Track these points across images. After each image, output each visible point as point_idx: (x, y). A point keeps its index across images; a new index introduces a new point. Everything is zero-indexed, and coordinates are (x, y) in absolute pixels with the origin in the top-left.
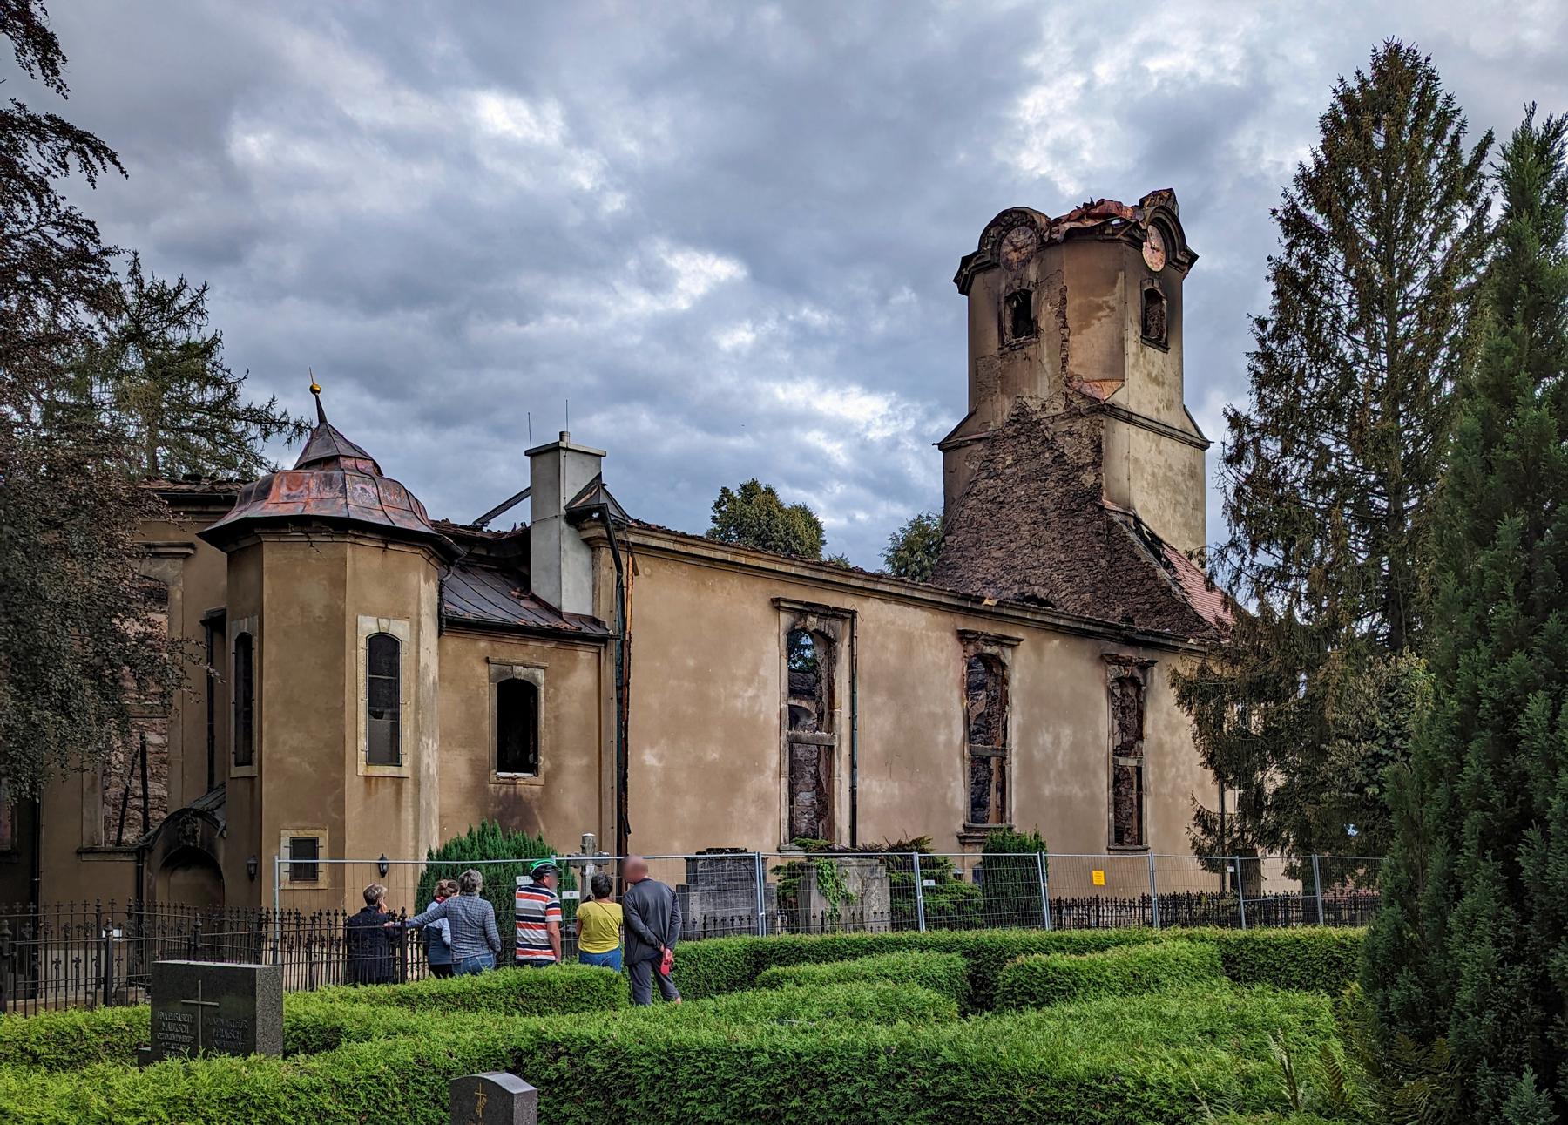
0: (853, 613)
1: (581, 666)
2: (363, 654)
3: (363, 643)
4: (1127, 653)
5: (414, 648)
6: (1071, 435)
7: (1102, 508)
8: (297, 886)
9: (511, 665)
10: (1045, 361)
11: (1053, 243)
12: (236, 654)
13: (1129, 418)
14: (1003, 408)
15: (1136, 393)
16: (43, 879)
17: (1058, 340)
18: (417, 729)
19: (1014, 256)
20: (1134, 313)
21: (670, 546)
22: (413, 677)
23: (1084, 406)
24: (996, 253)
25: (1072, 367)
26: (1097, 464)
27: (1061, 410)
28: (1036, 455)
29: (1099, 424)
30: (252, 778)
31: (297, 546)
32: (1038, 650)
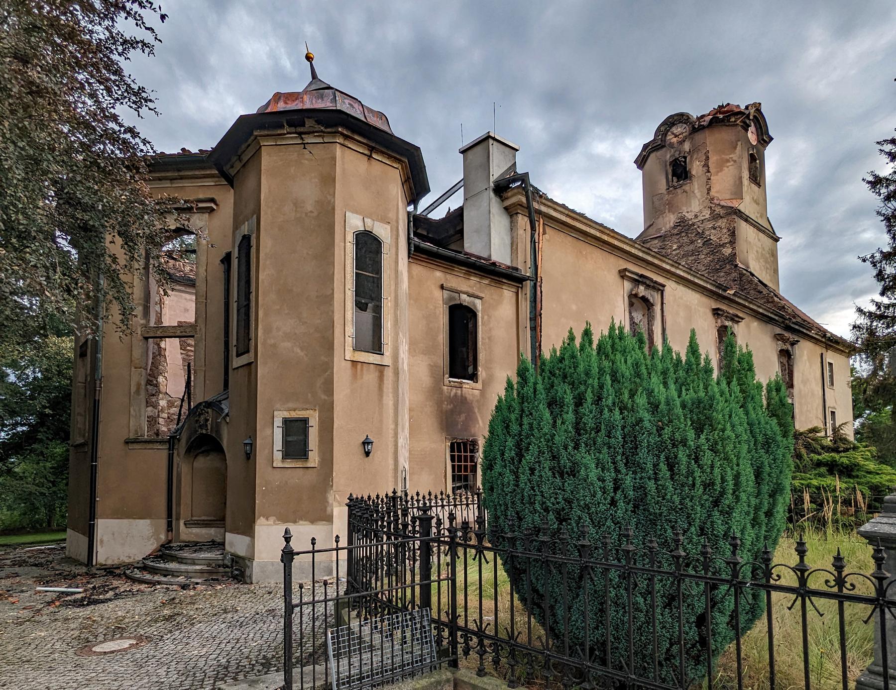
0: (664, 286)
1: (505, 301)
2: (351, 248)
3: (350, 238)
4: (787, 334)
5: (393, 250)
6: (715, 229)
7: (736, 266)
8: (289, 464)
9: (459, 292)
10: (696, 191)
11: (702, 128)
12: (239, 258)
13: (747, 219)
14: (669, 221)
15: (747, 206)
16: (100, 464)
17: (704, 179)
18: (396, 322)
19: (675, 140)
20: (745, 165)
21: (564, 218)
22: (393, 276)
23: (722, 212)
24: (663, 140)
25: (713, 193)
26: (732, 243)
27: (707, 216)
28: (692, 242)
29: (733, 221)
30: (250, 364)
31: (291, 148)
32: (748, 326)
